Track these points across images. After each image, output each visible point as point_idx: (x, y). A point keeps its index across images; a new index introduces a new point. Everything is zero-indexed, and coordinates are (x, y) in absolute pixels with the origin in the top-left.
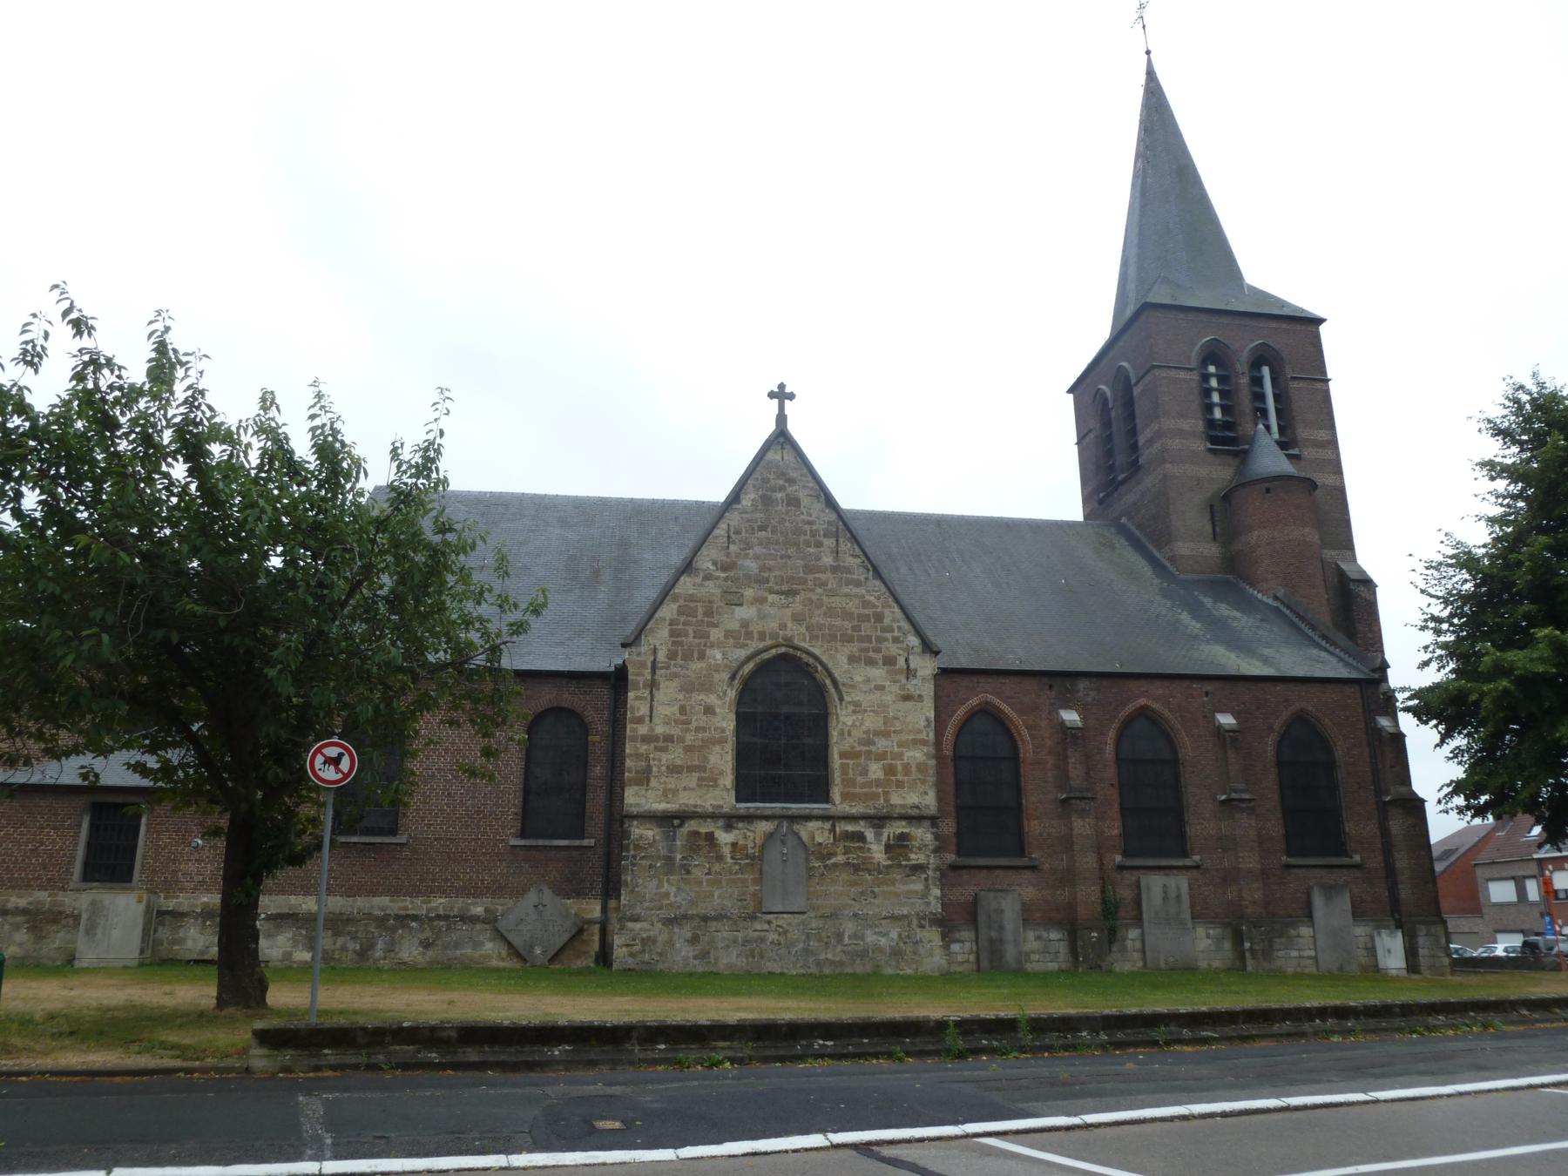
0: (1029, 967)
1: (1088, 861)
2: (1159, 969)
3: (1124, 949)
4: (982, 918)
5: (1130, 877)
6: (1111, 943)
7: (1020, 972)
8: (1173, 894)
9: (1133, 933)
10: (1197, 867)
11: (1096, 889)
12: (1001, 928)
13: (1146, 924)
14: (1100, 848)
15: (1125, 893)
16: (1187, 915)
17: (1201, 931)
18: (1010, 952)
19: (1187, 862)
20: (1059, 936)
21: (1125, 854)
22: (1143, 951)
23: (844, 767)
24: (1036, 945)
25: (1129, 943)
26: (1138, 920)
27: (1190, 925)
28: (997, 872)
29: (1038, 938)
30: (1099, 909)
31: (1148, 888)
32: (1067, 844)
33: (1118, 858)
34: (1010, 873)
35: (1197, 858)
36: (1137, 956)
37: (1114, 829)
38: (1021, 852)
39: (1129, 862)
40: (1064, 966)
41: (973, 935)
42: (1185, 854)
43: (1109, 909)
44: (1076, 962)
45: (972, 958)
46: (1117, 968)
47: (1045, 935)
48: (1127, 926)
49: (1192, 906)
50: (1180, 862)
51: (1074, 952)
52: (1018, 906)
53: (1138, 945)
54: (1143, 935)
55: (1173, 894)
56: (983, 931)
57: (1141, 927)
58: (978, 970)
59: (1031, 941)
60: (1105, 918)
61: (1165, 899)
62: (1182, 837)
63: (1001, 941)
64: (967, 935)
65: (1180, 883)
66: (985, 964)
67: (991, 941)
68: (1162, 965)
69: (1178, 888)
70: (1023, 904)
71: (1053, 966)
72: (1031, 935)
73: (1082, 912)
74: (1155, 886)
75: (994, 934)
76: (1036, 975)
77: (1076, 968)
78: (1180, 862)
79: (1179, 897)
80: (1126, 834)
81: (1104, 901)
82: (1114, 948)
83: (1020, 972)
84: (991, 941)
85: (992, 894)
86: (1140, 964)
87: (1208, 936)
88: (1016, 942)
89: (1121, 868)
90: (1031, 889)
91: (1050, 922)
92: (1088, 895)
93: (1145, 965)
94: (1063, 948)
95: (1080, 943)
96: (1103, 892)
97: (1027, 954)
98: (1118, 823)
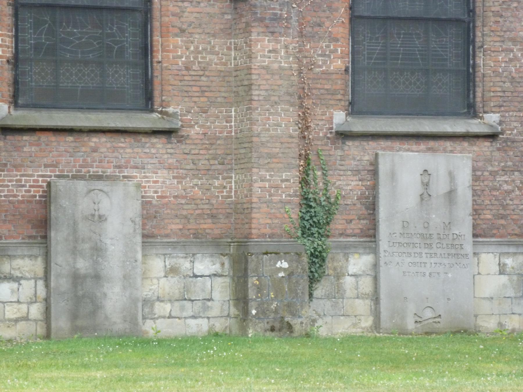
0: (149, 328)
1: (276, 123)
2: (403, 332)
3: (337, 294)
4: (58, 236)
5: (358, 153)
6: (313, 280)
7: (132, 338)
8: (440, 186)
9: (358, 263)
10: (492, 137)
11: (292, 176)
12: (98, 251)
13: (384, 244)
14: (303, 99)
15: (347, 186)
16: (465, 228)
17: (489, 260)
18: (114, 300)
19: (474, 126)
20: (216, 268)
21: (354, 109)
22: (376, 299)
23: (349, 64)
24: (168, 286)
25: (348, 281)
26: (370, 235)
27: (469, 248)
28: (95, 140)
29: (172, 271)
30: (295, 213)
31: (393, 175)
32: (240, 87)
33: (339, 117)
34: (123, 142)
35: (492, 118)
36: (363, 306)
37: (334, 58)
38: (147, 101)
39: (359, 125)
40: (219, 326)
41: (38, 266)
42: (471, 111)
43: (314, 217)
44: (244, 317)
45: (36, 311)
46: (323, 330)
47: (185, 265)
48: (347, 250)
49: (476, 212)
50: (460, 126)
51: (241, 299)
52: (134, 209)
53: (366, 285)
54: (376, 266)
55: (440, 186)
56: (61, 260)
57: (375, 251)
58: (48, 336)
59: (157, 277)
60: (306, 232)
61: (424, 197)
62: (468, 77)
63: (97, 277)
64: (28, 265)
65: (457, 167)
66: (61, 322)
67: (77, 278)
68: (411, 325)
69: (451, 176)
70: (146, 204)
71: (199, 326)
72: (157, 265)
73: (261, 221)
74: (405, 170)
75: (83, 265)
76: (331, 340)
77: (244, 330)
78: (460, 126)
79: (451, 195)
80: (355, 70)
81: (306, 202)
82: (319, 291)
83: (132, 338)
84: (77, 278)
85: (81, 186)
86: (368, 322)
87: (502, 272)
88: (127, 279)
89: (344, 136)
90: (163, 174)
91: (196, 241)
92: (272, 193)
93: (377, 326)
94: (221, 291)
95: (253, 281)
96: (304, 182)
97: (147, 302)
98: (343, 47)
